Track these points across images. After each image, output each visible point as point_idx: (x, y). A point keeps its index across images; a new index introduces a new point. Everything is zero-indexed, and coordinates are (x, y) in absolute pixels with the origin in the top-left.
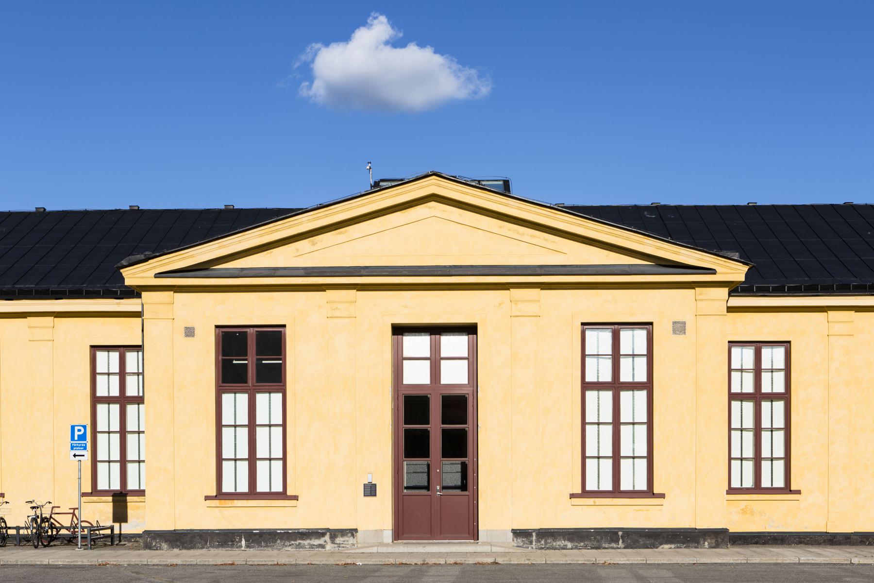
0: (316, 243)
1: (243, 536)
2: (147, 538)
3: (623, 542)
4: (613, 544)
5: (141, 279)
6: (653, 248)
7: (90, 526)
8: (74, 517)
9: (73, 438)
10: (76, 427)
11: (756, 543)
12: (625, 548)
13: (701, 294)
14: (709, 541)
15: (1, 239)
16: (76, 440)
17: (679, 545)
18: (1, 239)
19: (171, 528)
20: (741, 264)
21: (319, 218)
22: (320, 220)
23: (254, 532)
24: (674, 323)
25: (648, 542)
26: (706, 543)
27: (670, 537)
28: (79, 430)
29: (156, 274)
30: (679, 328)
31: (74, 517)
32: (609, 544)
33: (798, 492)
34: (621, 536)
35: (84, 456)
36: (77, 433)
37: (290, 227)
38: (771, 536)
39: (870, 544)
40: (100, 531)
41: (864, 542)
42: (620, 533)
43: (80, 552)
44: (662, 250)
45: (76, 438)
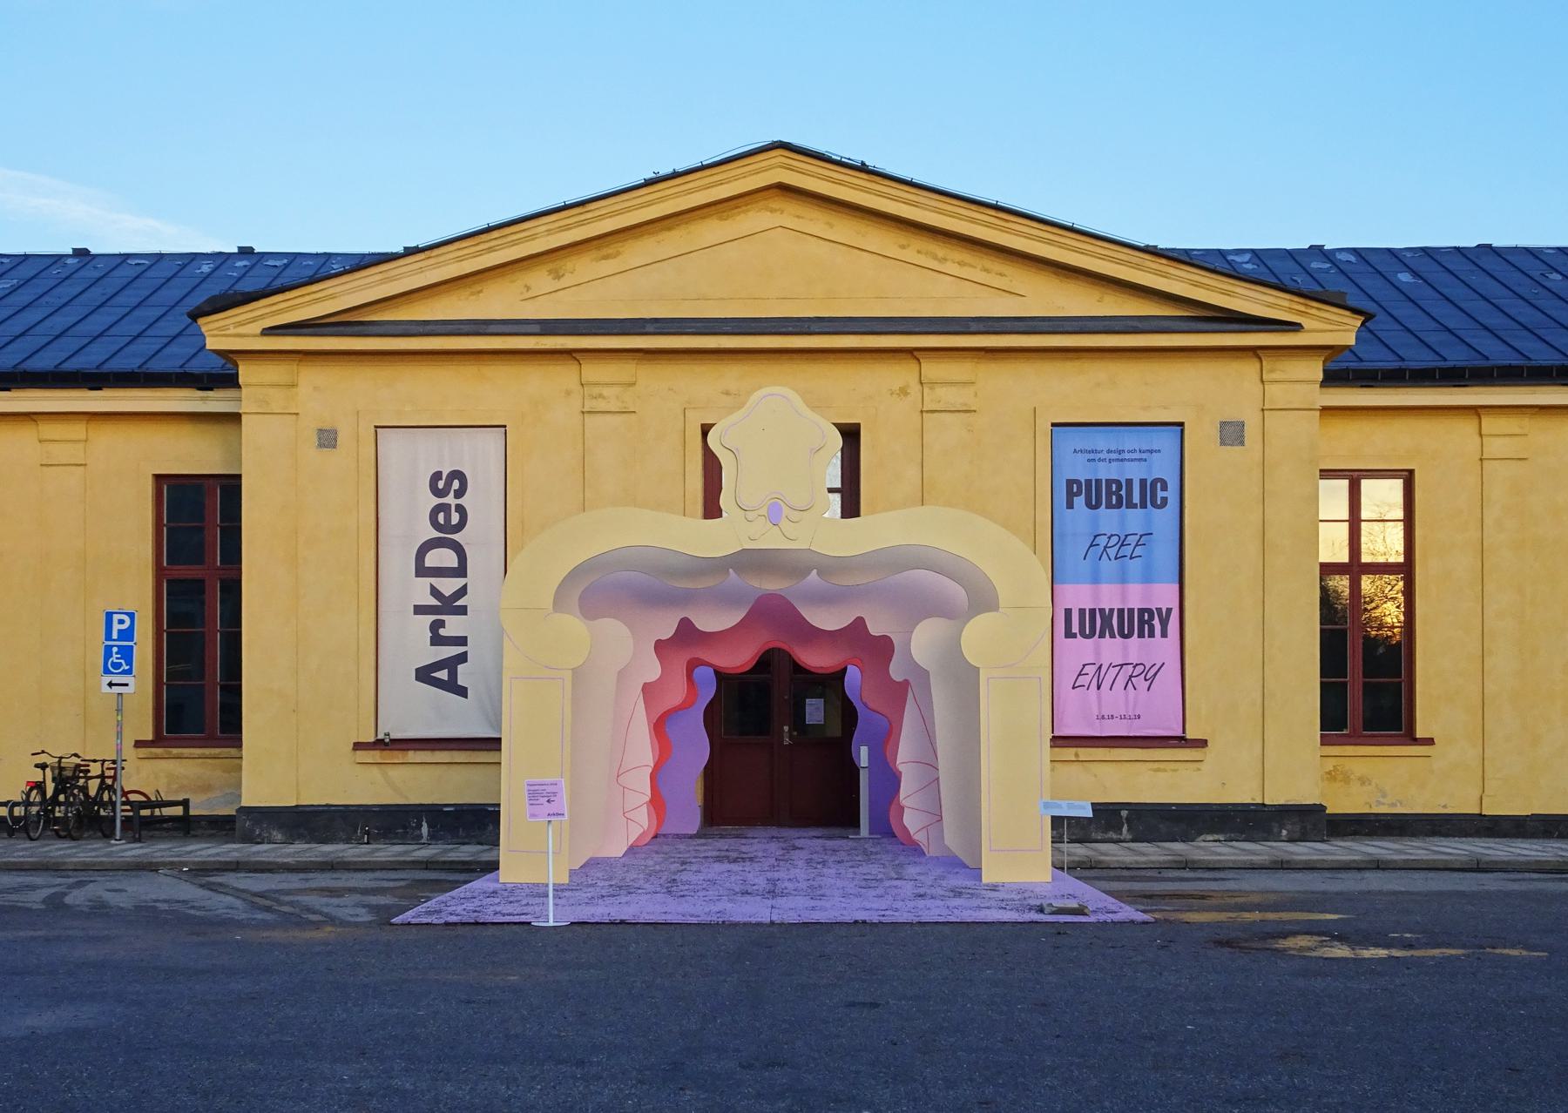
0: (563, 275)
1: (424, 820)
2: (245, 821)
3: (1128, 830)
4: (1111, 833)
5: (238, 339)
6: (1187, 285)
7: (145, 799)
8: (1082, 673)
9: (108, 636)
10: (114, 615)
11: (1355, 833)
12: (1133, 841)
13: (1272, 371)
14: (1289, 827)
15: (3, 347)
16: (114, 640)
17: (1233, 835)
18: (3, 347)
19: (291, 802)
20: (1348, 313)
21: (567, 228)
22: (571, 231)
23: (490, 809)
24: (1223, 424)
25: (1176, 829)
26: (1284, 832)
27: (1216, 820)
28: (121, 622)
29: (264, 329)
30: (1232, 433)
31: (1082, 673)
32: (1103, 832)
33: (1429, 742)
34: (1127, 819)
35: (127, 685)
36: (116, 627)
37: (514, 243)
38: (1379, 821)
39: (1562, 836)
40: (163, 809)
41: (1550, 832)
42: (1124, 813)
43: (119, 847)
44: (1202, 287)
45: (115, 636)
